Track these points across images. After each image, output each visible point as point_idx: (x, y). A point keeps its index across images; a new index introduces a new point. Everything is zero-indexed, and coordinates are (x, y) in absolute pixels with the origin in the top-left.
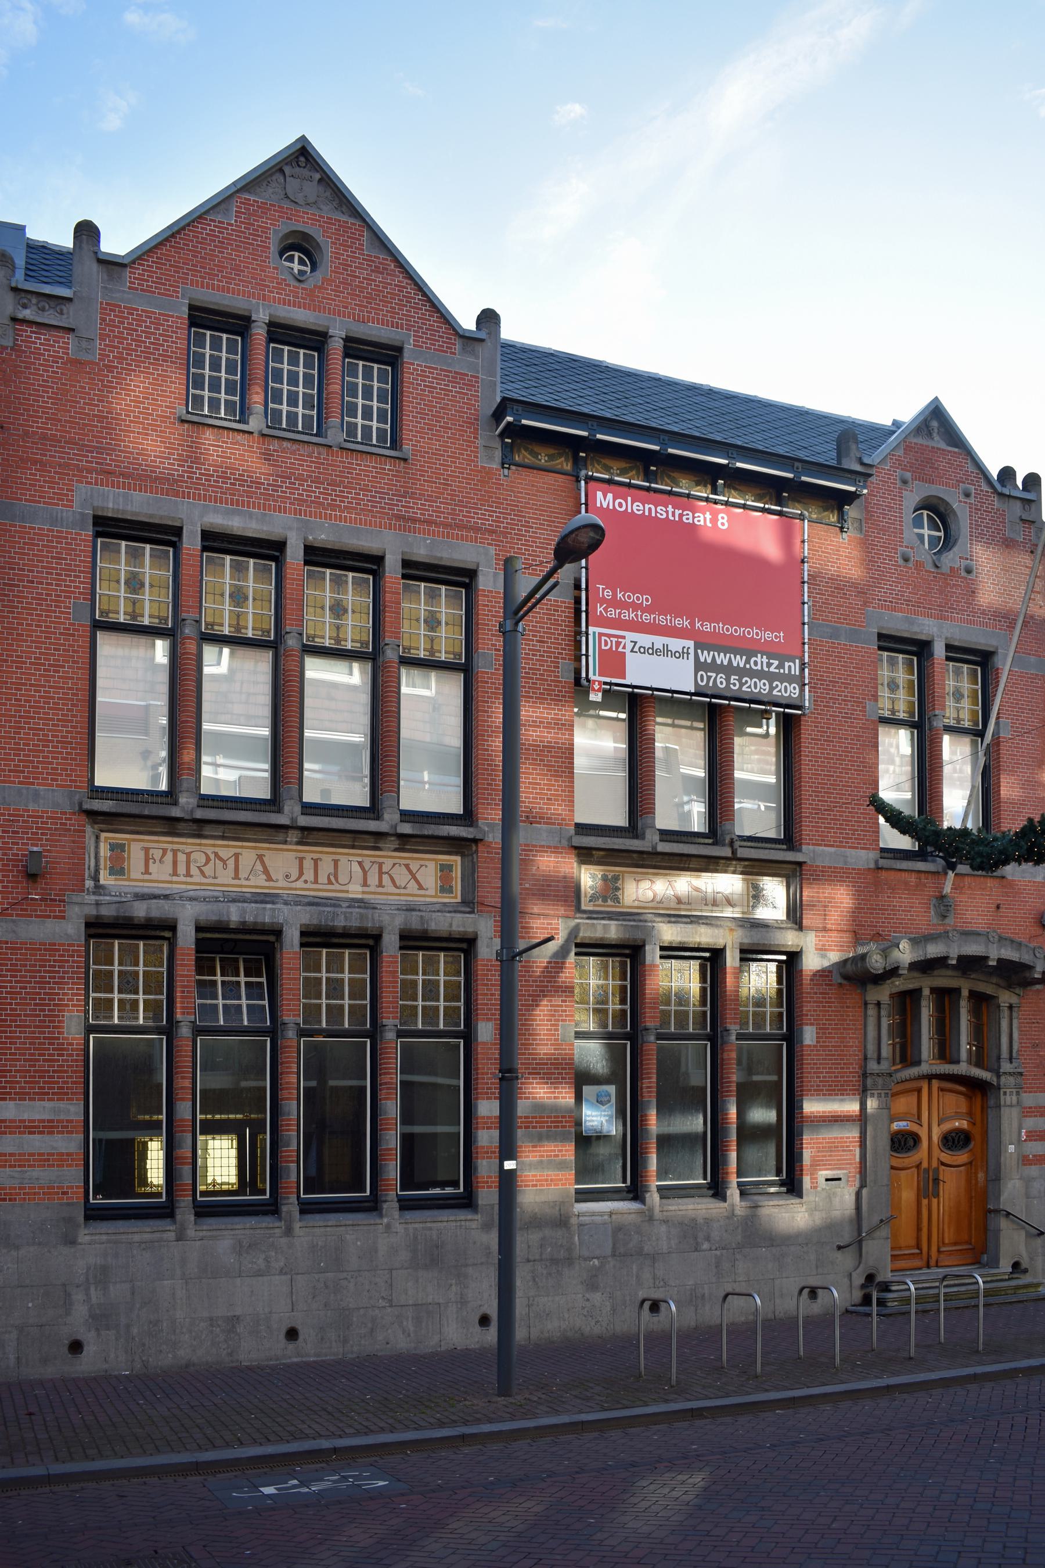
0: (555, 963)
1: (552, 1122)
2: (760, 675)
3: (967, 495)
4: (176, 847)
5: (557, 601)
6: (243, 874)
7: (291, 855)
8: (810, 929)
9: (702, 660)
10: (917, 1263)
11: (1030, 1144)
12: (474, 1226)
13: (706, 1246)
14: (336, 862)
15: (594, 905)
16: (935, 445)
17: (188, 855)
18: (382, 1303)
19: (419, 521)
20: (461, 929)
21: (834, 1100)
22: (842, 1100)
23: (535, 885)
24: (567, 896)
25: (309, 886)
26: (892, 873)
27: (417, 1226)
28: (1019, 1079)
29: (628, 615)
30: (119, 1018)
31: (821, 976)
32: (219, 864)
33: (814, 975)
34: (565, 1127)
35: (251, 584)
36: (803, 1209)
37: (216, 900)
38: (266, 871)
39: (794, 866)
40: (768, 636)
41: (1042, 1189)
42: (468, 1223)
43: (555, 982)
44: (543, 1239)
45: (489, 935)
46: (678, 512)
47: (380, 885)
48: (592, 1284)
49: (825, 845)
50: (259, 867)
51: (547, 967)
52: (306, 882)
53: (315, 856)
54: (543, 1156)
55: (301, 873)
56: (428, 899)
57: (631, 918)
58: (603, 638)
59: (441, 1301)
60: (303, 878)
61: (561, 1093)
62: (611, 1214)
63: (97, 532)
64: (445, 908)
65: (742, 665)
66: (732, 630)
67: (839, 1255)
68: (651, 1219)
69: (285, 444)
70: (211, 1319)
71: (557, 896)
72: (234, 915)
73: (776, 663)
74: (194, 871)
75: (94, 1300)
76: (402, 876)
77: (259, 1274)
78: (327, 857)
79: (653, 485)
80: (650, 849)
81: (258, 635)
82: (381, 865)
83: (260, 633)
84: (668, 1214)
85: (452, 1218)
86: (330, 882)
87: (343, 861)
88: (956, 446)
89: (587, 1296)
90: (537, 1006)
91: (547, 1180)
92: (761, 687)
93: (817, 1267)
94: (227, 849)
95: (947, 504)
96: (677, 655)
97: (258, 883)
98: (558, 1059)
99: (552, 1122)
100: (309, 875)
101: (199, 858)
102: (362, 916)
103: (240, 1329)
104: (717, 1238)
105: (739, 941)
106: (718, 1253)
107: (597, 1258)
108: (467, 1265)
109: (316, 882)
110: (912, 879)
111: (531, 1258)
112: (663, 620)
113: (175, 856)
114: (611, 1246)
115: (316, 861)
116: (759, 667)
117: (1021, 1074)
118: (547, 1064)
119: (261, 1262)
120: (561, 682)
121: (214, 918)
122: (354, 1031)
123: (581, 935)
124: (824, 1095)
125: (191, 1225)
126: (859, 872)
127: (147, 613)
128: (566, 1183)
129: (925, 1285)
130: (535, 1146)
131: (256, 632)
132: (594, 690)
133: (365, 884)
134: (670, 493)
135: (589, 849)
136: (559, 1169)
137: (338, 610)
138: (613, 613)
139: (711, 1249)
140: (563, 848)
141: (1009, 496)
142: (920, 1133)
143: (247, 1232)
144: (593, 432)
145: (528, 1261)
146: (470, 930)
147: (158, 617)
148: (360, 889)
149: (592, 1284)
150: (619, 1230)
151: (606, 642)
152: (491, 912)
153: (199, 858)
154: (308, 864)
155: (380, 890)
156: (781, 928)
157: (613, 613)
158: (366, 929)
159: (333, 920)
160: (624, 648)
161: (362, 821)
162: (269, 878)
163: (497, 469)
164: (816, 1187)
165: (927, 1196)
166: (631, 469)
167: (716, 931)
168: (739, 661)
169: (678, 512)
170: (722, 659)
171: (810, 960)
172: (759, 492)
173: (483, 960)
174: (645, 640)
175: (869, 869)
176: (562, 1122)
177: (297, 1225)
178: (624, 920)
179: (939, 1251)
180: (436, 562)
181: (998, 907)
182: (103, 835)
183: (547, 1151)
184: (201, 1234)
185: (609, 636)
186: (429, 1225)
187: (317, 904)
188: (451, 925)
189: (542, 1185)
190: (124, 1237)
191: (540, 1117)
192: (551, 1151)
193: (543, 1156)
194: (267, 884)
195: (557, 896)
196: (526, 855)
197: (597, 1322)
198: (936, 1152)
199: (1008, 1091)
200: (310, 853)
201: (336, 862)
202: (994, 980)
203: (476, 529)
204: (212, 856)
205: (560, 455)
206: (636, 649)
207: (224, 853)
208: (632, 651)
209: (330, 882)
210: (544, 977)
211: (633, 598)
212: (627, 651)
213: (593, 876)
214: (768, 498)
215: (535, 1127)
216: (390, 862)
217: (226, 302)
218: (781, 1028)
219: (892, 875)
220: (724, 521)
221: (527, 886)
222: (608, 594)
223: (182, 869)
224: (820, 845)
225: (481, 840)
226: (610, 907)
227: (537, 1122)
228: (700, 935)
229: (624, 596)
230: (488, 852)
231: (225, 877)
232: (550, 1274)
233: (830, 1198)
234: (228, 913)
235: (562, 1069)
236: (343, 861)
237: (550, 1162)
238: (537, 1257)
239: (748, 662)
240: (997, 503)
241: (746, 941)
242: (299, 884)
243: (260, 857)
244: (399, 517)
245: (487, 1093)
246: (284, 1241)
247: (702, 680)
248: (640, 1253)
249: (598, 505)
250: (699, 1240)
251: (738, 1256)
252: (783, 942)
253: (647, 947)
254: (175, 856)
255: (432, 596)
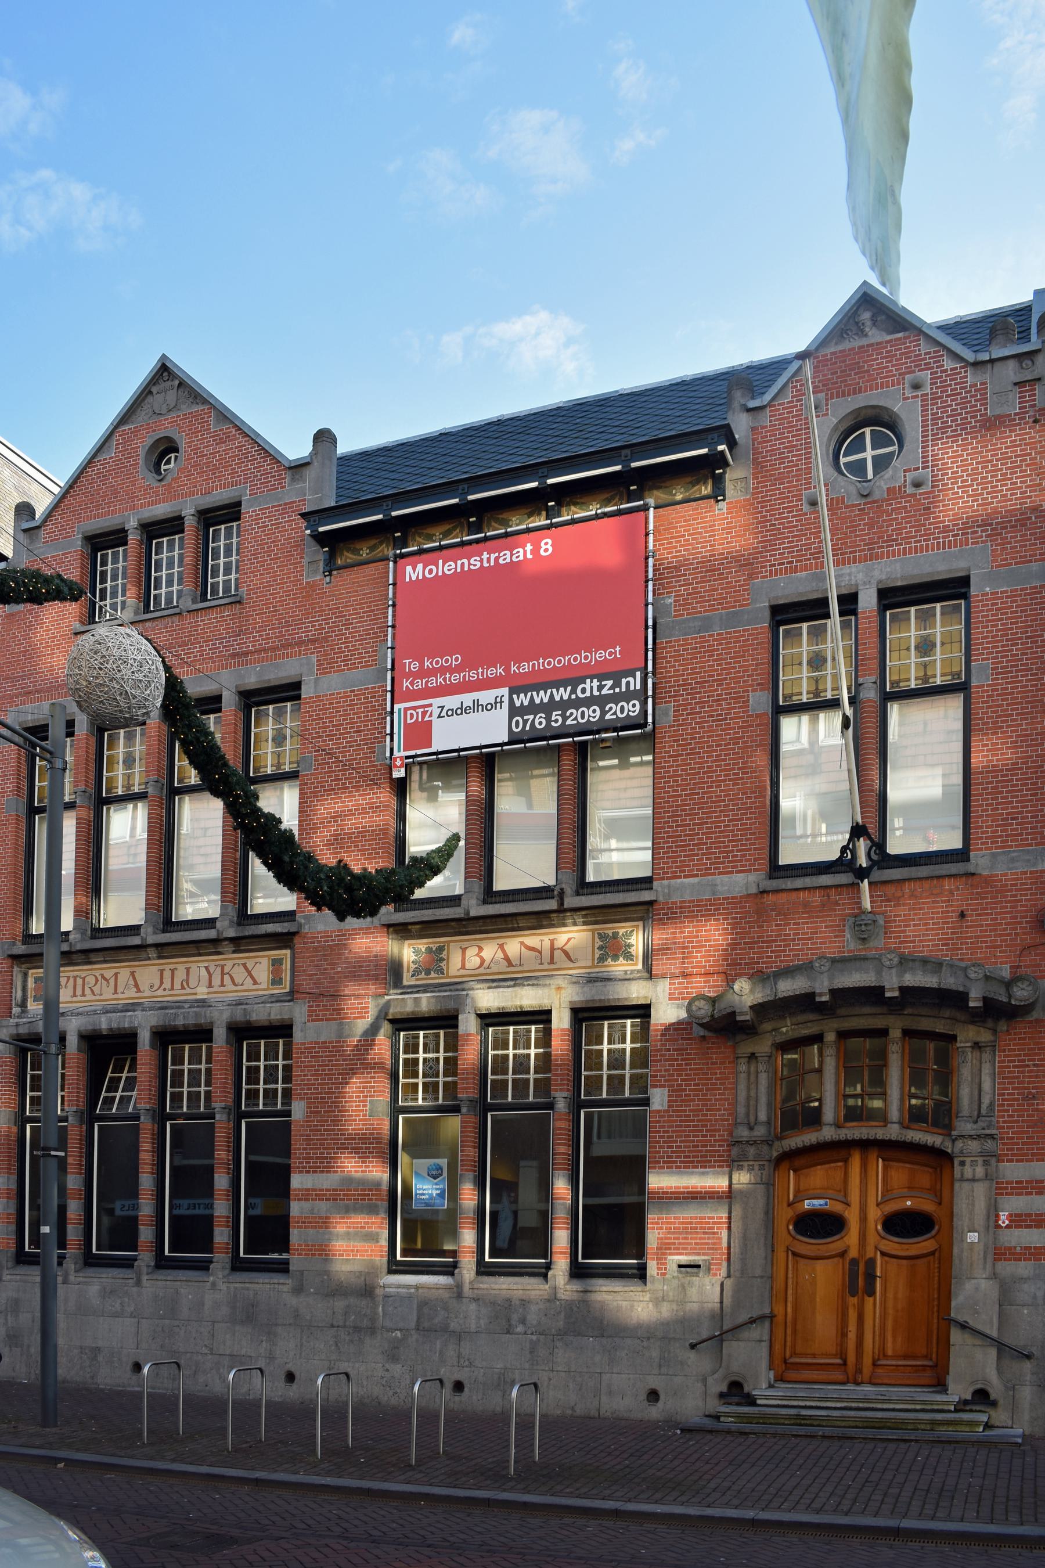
0: (365, 1041)
1: (359, 1195)
2: (588, 702)
3: (916, 387)
4: (75, 974)
5: (374, 688)
6: (119, 990)
7: (155, 969)
8: (664, 976)
9: (518, 704)
10: (839, 1376)
11: (1017, 1232)
12: (285, 1290)
13: (520, 1329)
14: (188, 970)
15: (417, 980)
16: (872, 341)
17: (84, 979)
18: (205, 1350)
19: (264, 650)
20: (279, 1017)
21: (692, 1173)
22: (703, 1173)
23: (347, 968)
24: (378, 975)
25: (168, 992)
26: (784, 895)
27: (237, 1285)
28: (989, 1145)
29: (434, 682)
30: (264, 1104)
31: (675, 1029)
32: (104, 983)
33: (666, 1029)
34: (371, 1200)
35: (938, 630)
36: (647, 1297)
37: (87, 1014)
38: (136, 985)
39: (646, 907)
40: (601, 655)
41: (1040, 1294)
42: (281, 1286)
43: (364, 1059)
44: (348, 1306)
45: (303, 1020)
46: (493, 556)
47: (222, 985)
48: (392, 1356)
49: (685, 877)
50: (132, 982)
51: (357, 1046)
52: (165, 989)
53: (172, 967)
54: (349, 1227)
55: (162, 983)
56: (261, 993)
57: (451, 987)
58: (409, 712)
59: (253, 1355)
60: (164, 986)
61: (368, 1167)
62: (417, 1287)
63: (885, 605)
64: (278, 999)
65: (565, 697)
66: (554, 663)
67: (692, 1355)
68: (460, 1296)
69: (148, 624)
70: (81, 1348)
71: (368, 975)
72: (104, 1023)
73: (610, 683)
74: (87, 991)
75: (10, 1324)
76: (239, 974)
77: (116, 1315)
78: (180, 966)
79: (554, 521)
80: (462, 916)
81: (948, 680)
82: (223, 967)
83: (949, 678)
84: (480, 1292)
85: (266, 1281)
86: (183, 988)
87: (194, 967)
88: (904, 329)
89: (387, 1366)
90: (347, 1083)
91: (353, 1251)
92: (593, 714)
93: (660, 1366)
94: (108, 970)
95: (886, 409)
96: (489, 707)
97: (130, 994)
98: (365, 1134)
99: (359, 1195)
100: (167, 984)
101: (91, 980)
102: (197, 1014)
103: (100, 1358)
104: (535, 1322)
105: (569, 999)
106: (534, 1338)
107: (400, 1330)
108: (276, 1325)
109: (172, 989)
110: (817, 898)
111: (335, 1324)
112: (473, 675)
113: (75, 981)
114: (415, 1319)
115: (173, 971)
116: (588, 694)
117: (991, 1137)
118: (355, 1139)
119: (118, 1306)
120: (376, 766)
121: (90, 1028)
122: (448, 1106)
123: (391, 1011)
124: (660, 1168)
125: (72, 1272)
126: (735, 902)
127: (137, 783)
128: (376, 1253)
129: (808, 1403)
130: (343, 1218)
131: (944, 678)
132: (396, 766)
133: (210, 986)
134: (507, 535)
135: (405, 925)
136: (365, 1241)
137: (925, 647)
138: (419, 684)
139: (525, 1333)
140: (375, 928)
141: (992, 361)
142: (846, 1214)
143: (110, 1280)
144: (387, 513)
145: (332, 1326)
146: (286, 1017)
147: (952, 674)
148: (206, 990)
149: (392, 1356)
150: (424, 1304)
151: (412, 716)
152: (305, 998)
153: (91, 980)
154: (167, 974)
155: (222, 989)
156: (629, 979)
157: (419, 684)
158: (201, 1025)
159: (174, 1020)
160: (431, 715)
161: (633, 893)
162: (139, 991)
163: (320, 580)
164: (664, 1274)
165: (853, 1293)
166: (455, 528)
167: (540, 992)
168: (562, 694)
169: (493, 556)
170: (542, 697)
171: (661, 1013)
172: (689, 479)
173: (297, 1044)
174: (452, 702)
175: (749, 895)
176: (368, 1195)
177: (145, 1278)
178: (440, 991)
179: (874, 1365)
180: (266, 685)
181: (962, 915)
182: (31, 971)
183: (354, 1223)
184: (78, 1279)
185: (414, 708)
186: (247, 1285)
187: (165, 1008)
188: (270, 1014)
189: (349, 1255)
190: (30, 1278)
191: (348, 1190)
192: (358, 1223)
193: (349, 1227)
194: (137, 995)
195: (368, 975)
196: (341, 940)
197: (395, 1393)
198: (872, 1239)
199: (968, 1160)
200: (169, 964)
201: (188, 970)
202: (947, 1013)
203: (300, 643)
204: (99, 978)
205: (381, 543)
206: (444, 713)
207: (109, 974)
208: (439, 717)
209: (183, 988)
210: (354, 1055)
211: (442, 662)
212: (434, 718)
213: (417, 952)
214: (617, 499)
215: (343, 1200)
216: (229, 964)
217: (107, 524)
218: (437, 1099)
219: (783, 897)
220: (544, 547)
221: (339, 969)
222: (415, 666)
223: (79, 992)
224: (680, 877)
225: (297, 933)
226: (434, 979)
227: (344, 1195)
228: (521, 998)
229: (431, 663)
230: (304, 943)
231: (108, 994)
232: (352, 1341)
233: (684, 1288)
234: (100, 1022)
235: (370, 1143)
236: (194, 967)
237: (356, 1234)
238: (341, 1324)
239: (574, 691)
240: (971, 377)
241: (576, 998)
242: (160, 992)
243: (133, 974)
244: (233, 656)
245: (298, 1167)
246: (135, 1289)
247: (517, 726)
248: (445, 1329)
249: (407, 580)
250: (513, 1323)
251: (559, 1344)
252: (625, 996)
253: (460, 1017)
254: (75, 981)
255: (926, 619)
